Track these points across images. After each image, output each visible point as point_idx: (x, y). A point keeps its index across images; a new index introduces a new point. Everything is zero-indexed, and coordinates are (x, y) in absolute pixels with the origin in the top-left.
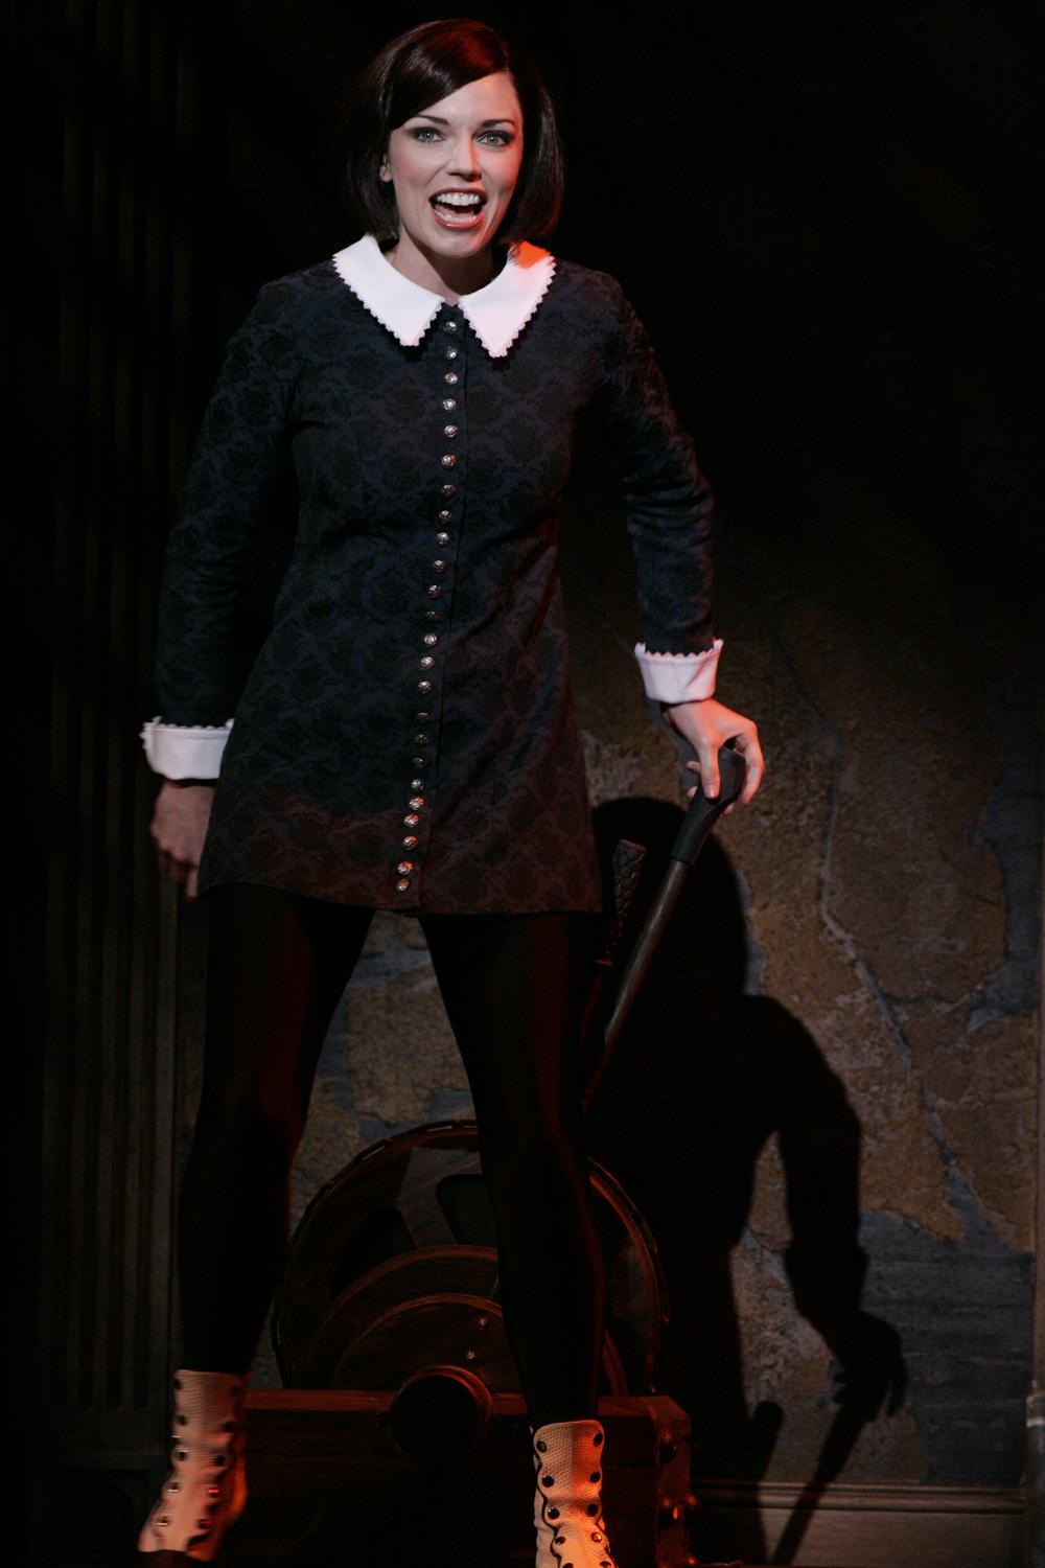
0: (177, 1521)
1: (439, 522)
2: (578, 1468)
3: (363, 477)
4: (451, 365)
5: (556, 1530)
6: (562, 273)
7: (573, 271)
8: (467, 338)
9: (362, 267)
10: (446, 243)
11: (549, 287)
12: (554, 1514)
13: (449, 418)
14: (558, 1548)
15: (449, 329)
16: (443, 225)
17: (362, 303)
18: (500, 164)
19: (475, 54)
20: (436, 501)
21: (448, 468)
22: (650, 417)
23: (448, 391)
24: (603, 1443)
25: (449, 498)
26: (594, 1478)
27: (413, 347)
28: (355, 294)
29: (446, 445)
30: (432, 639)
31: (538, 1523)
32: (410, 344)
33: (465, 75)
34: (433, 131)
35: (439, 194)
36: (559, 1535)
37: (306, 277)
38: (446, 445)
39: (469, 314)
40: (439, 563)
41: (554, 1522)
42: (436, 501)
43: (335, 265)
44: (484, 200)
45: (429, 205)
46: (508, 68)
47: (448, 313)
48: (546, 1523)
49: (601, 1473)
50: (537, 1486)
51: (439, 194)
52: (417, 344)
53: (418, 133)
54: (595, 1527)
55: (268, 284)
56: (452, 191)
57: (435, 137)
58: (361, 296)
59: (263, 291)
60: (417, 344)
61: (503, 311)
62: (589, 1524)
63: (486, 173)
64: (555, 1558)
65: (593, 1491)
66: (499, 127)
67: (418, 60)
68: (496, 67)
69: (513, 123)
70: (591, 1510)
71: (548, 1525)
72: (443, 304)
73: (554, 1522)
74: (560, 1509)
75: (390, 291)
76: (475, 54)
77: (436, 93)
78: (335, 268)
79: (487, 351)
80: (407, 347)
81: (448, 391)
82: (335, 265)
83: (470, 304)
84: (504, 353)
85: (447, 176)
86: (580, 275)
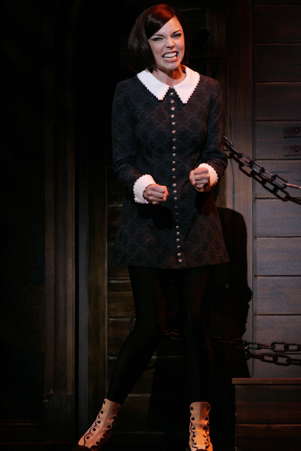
0: (94, 435)
1: (173, 150)
2: (202, 417)
3: (150, 138)
4: (172, 105)
5: (194, 433)
6: (202, 79)
7: (206, 78)
8: (176, 97)
9: (145, 77)
10: (170, 66)
11: (198, 84)
12: (194, 429)
13: (173, 120)
14: (194, 438)
15: (172, 94)
16: (168, 62)
17: (146, 88)
18: (180, 42)
19: (165, 13)
20: (171, 144)
21: (174, 134)
22: (217, 139)
23: (171, 112)
24: (210, 409)
25: (174, 143)
26: (206, 419)
27: (161, 100)
28: (144, 85)
29: (173, 128)
30: (175, 185)
31: (190, 431)
32: (161, 100)
33: (165, 20)
34: (159, 38)
35: (165, 54)
36: (194, 435)
37: (130, 81)
38: (173, 128)
39: (176, 91)
40: (174, 162)
41: (194, 431)
42: (171, 144)
43: (138, 76)
44: (177, 53)
45: (162, 58)
46: (175, 15)
47: (171, 90)
48: (191, 431)
49: (209, 418)
50: (190, 420)
51: (165, 54)
52: (162, 99)
53: (156, 39)
54: (205, 433)
55: (119, 83)
56: (169, 53)
57: (160, 39)
58: (146, 86)
59: (118, 85)
60: (162, 99)
61: (188, 84)
62: (203, 432)
63: (176, 45)
64: (193, 441)
65: (206, 422)
66: (177, 33)
67: (150, 18)
68: (173, 16)
69: (180, 31)
70: (205, 428)
71: (192, 432)
72: (169, 88)
73: (194, 431)
74: (196, 427)
75: (154, 84)
76: (165, 13)
77: (158, 27)
78: (138, 77)
79: (182, 101)
80: (160, 100)
81: (171, 112)
82: (138, 76)
83: (176, 87)
84: (187, 102)
85: (166, 48)
86: (207, 79)
